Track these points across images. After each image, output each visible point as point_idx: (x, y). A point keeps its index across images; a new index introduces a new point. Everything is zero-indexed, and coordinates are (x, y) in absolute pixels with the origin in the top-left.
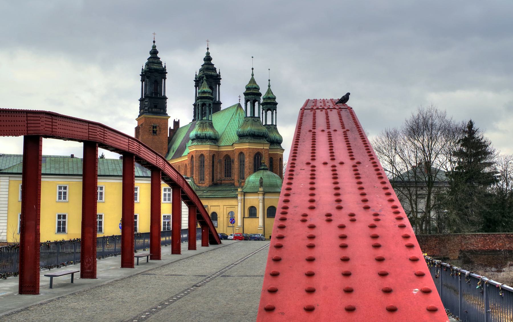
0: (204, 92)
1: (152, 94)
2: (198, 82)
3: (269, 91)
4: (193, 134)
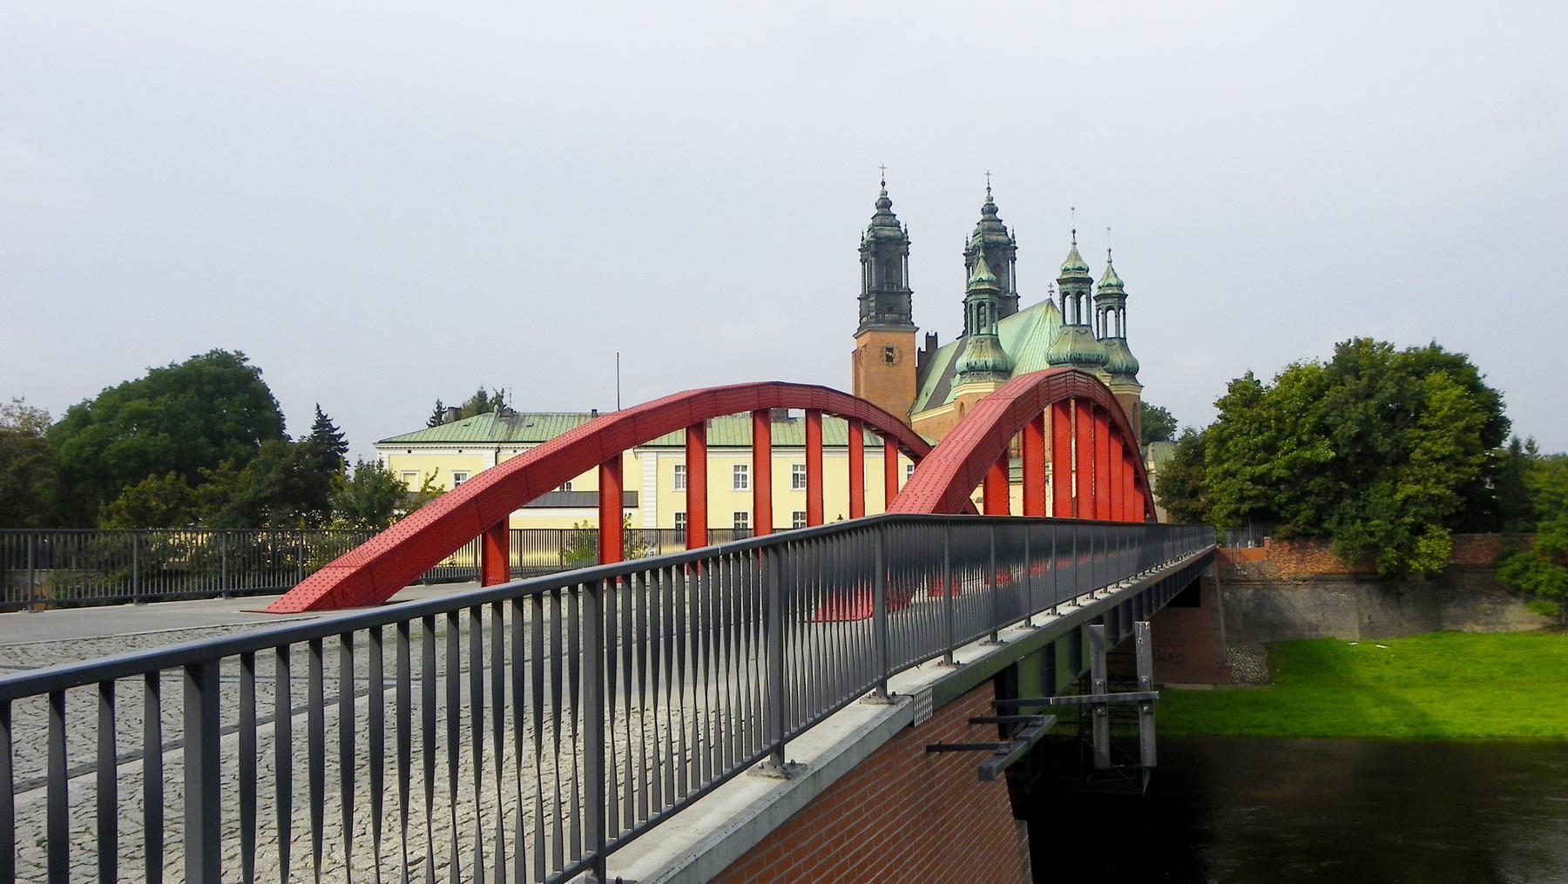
0: (981, 281)
1: (880, 284)
2: (970, 257)
3: (1111, 271)
4: (961, 363)
